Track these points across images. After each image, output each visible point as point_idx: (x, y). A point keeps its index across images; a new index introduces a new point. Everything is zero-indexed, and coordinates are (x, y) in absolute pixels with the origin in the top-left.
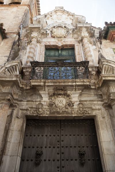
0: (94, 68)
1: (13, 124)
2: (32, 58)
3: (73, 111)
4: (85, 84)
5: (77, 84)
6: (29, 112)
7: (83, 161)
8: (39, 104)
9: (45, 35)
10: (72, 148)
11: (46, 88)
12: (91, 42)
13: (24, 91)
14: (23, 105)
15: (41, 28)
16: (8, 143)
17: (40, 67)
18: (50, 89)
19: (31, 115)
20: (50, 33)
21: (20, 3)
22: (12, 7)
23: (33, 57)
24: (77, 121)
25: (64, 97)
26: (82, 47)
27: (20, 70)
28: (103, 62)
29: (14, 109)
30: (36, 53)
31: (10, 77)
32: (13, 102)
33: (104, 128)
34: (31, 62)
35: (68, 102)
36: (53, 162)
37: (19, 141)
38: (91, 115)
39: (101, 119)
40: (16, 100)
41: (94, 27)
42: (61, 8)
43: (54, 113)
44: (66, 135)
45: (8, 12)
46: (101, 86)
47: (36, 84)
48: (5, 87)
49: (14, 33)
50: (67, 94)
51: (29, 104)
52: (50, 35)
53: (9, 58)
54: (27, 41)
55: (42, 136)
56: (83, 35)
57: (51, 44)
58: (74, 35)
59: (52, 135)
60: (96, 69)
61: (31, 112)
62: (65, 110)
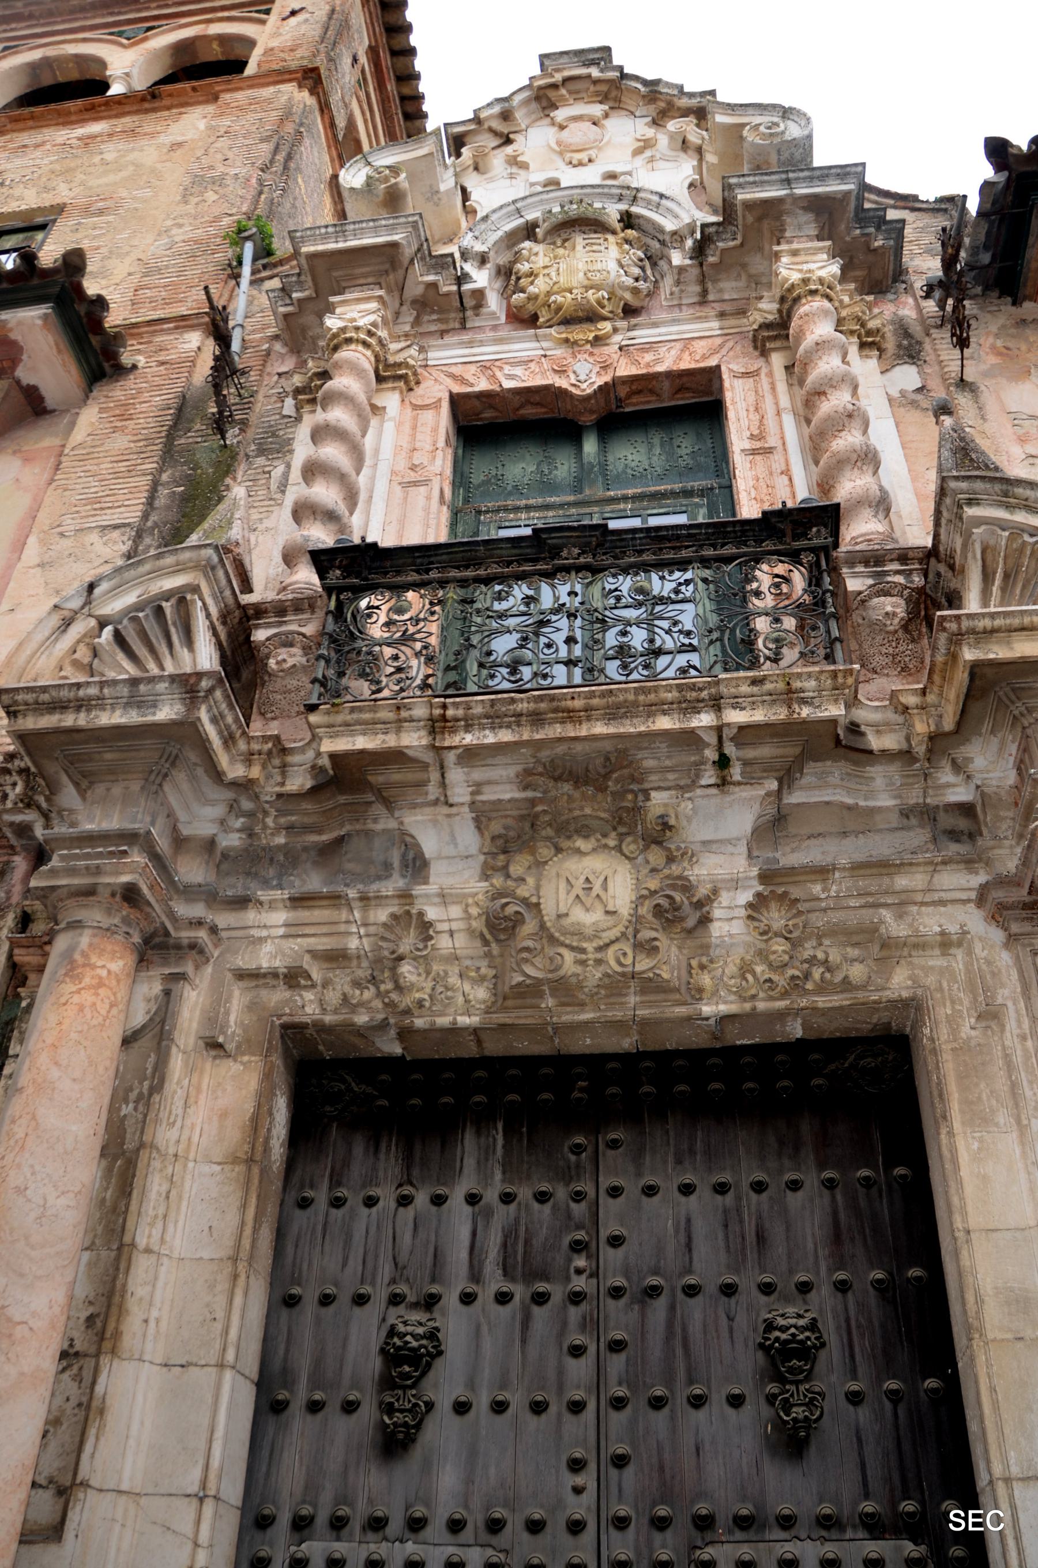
0: (895, 566)
1: (179, 1103)
2: (330, 516)
3: (702, 967)
4: (805, 712)
5: (735, 717)
6: (309, 995)
7: (798, 1412)
8: (394, 917)
9: (449, 310)
10: (699, 1299)
11: (456, 775)
12: (869, 333)
13: (266, 813)
14: (264, 933)
15: (408, 252)
16: (141, 1266)
17: (398, 589)
18: (489, 782)
19: (328, 1019)
20: (498, 284)
21: (244, 64)
22: (168, 108)
23: (342, 508)
25: (619, 849)
26: (790, 385)
27: (220, 628)
28: (970, 502)
29: (181, 977)
30: (365, 471)
31: (135, 702)
32: (171, 915)
33: (993, 1111)
34: (321, 559)
35: (653, 893)
36: (533, 1422)
37: (229, 1242)
39: (968, 1028)
40: (189, 892)
41: (887, 194)
42: (593, 63)
43: (529, 991)
44: (650, 1191)
45: (131, 157)
46: (959, 724)
47: (361, 743)
48: (100, 789)
49: (183, 318)
52: (494, 302)
53: (139, 536)
54: (297, 380)
55: (438, 1200)
56: (795, 277)
57: (508, 384)
58: (715, 281)
59: (524, 1193)
60: (907, 574)
61: (333, 997)
62: (628, 961)
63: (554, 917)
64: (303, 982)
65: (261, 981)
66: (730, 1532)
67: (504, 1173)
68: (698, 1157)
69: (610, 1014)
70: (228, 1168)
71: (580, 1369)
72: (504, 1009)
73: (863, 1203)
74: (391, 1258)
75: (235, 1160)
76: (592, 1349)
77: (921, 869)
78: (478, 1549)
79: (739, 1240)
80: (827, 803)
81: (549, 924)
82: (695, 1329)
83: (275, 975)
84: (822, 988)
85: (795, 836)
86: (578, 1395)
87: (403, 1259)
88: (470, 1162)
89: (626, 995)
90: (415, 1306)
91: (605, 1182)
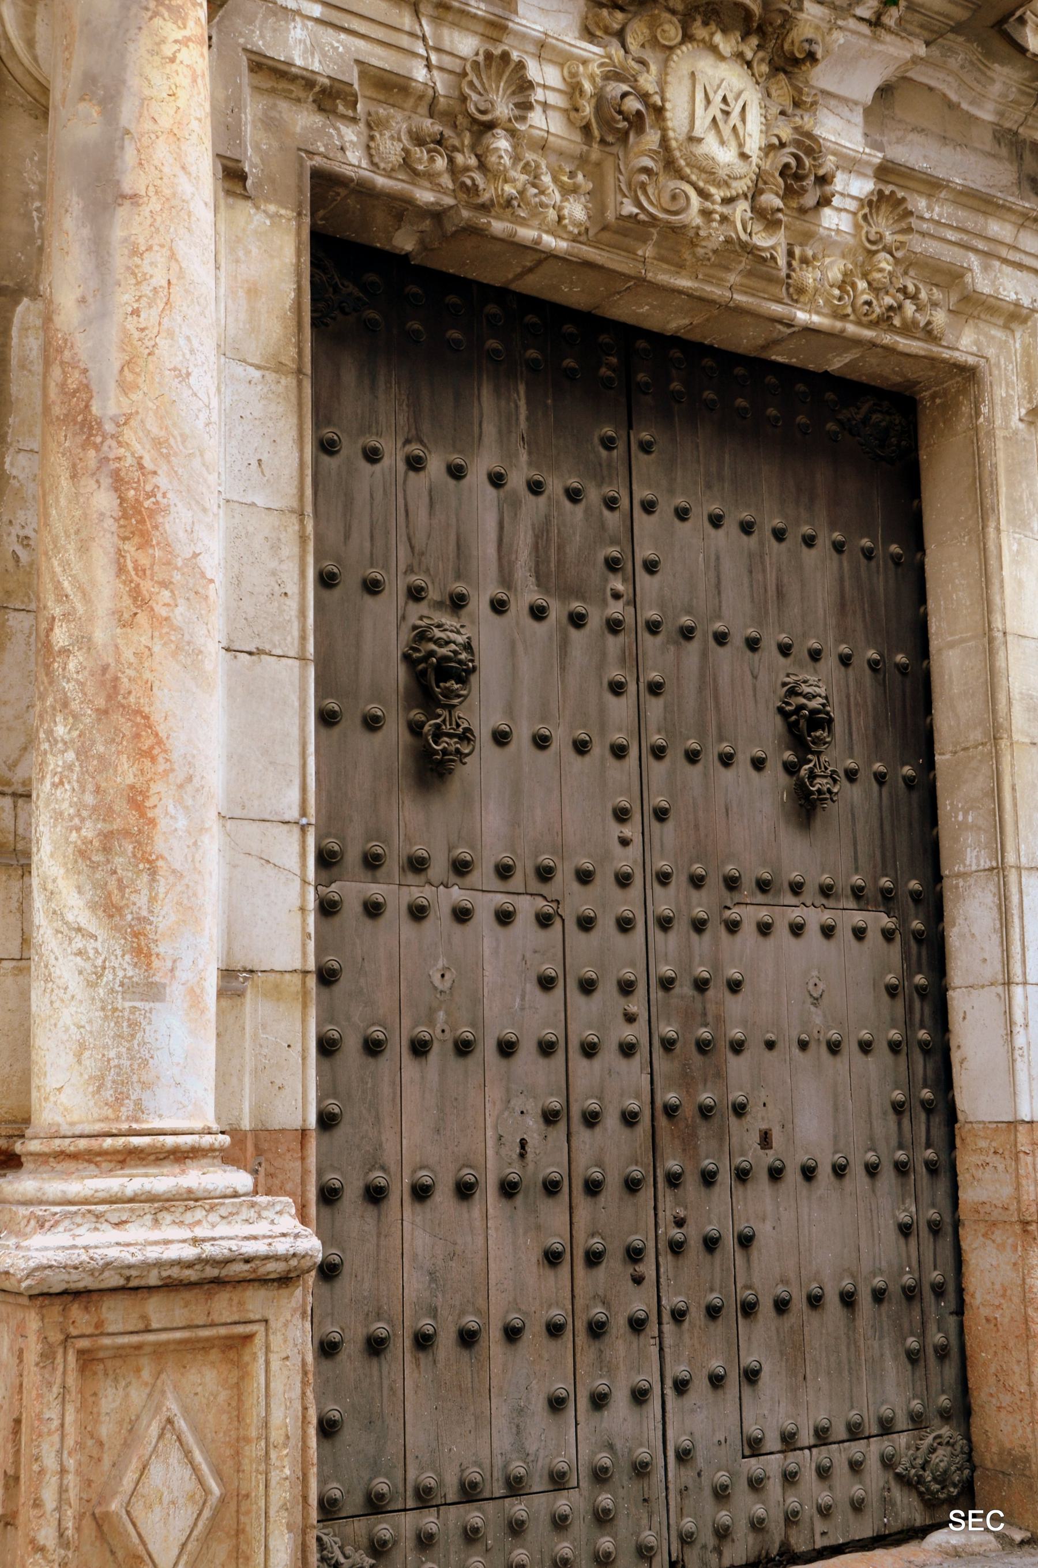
6: (350, 134)
24: (771, 379)
36: (577, 764)
38: (946, 354)
43: (634, 228)
50: (782, 37)
51: (356, 25)
59: (555, 486)
61: (391, 149)
63: (682, 137)
64: (341, 108)
65: (283, 85)
66: (753, 894)
67: (530, 453)
68: (726, 485)
69: (708, 288)
70: (271, 376)
71: (621, 708)
72: (595, 244)
73: (864, 575)
74: (405, 538)
75: (279, 368)
76: (632, 688)
77: (1013, 218)
78: (528, 897)
79: (762, 591)
80: (931, 89)
81: (674, 144)
82: (724, 681)
83: (309, 83)
84: (908, 329)
85: (900, 121)
86: (619, 737)
87: (420, 539)
88: (490, 430)
89: (727, 269)
90: (439, 605)
91: (643, 493)
